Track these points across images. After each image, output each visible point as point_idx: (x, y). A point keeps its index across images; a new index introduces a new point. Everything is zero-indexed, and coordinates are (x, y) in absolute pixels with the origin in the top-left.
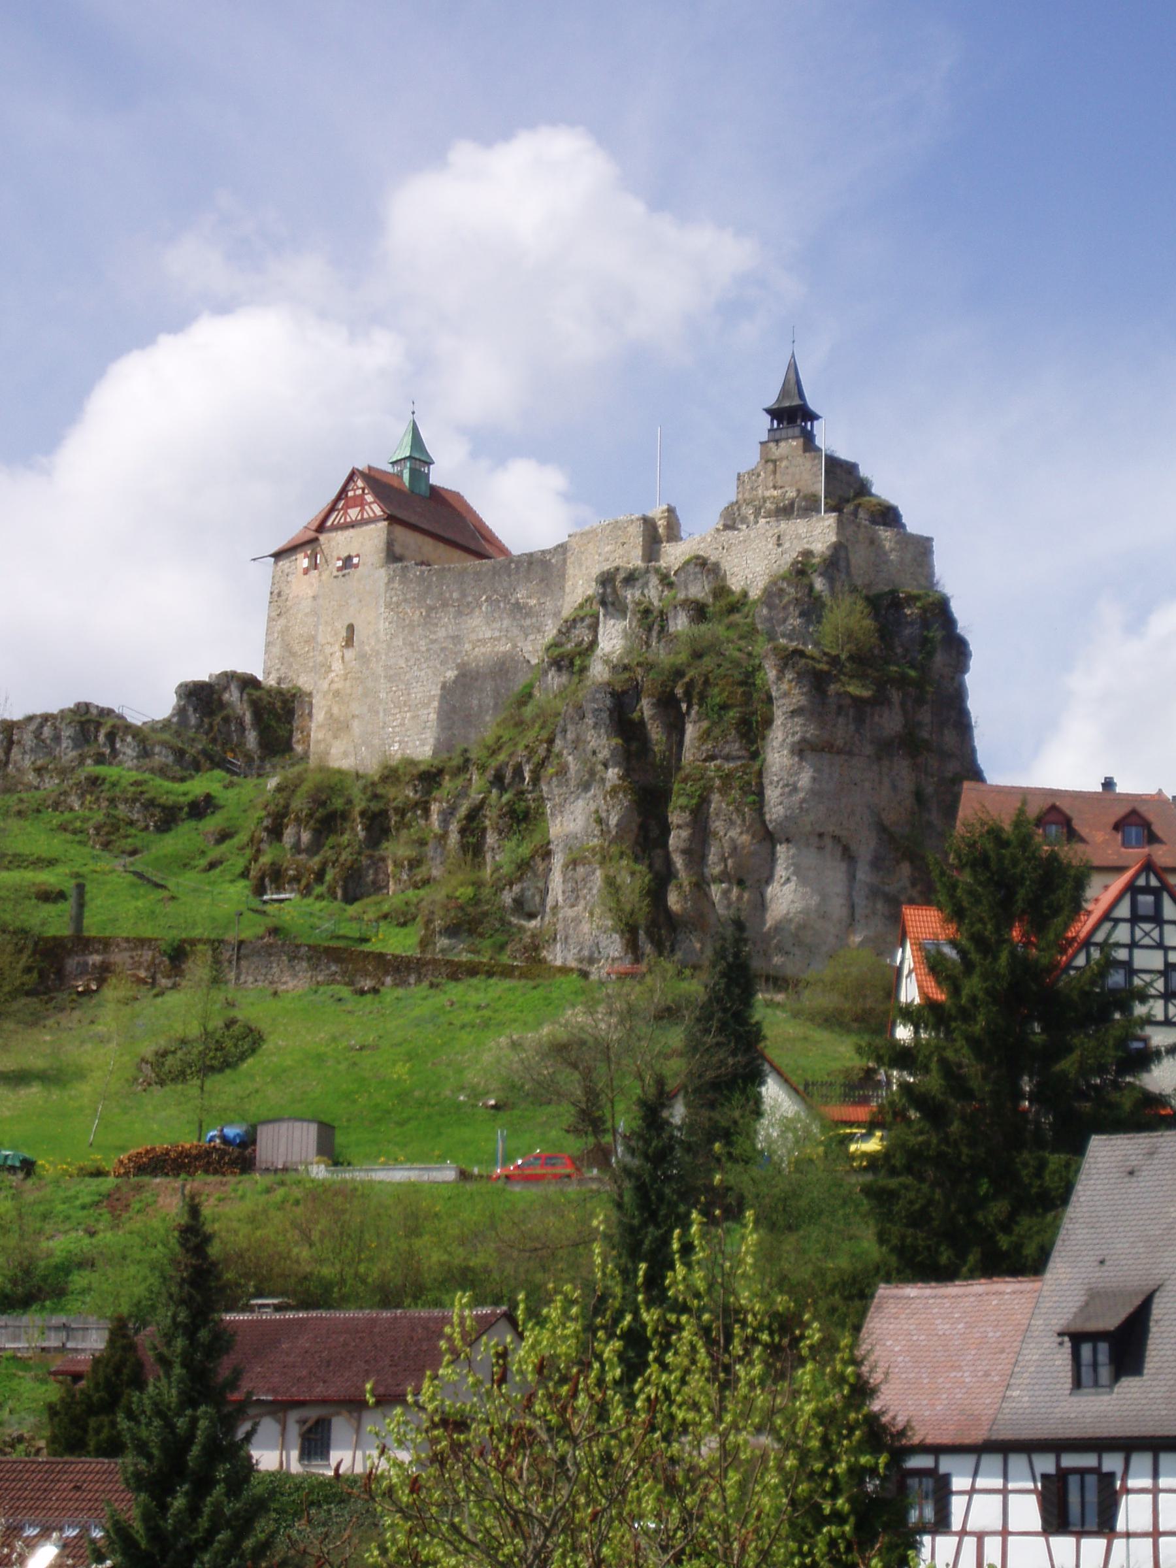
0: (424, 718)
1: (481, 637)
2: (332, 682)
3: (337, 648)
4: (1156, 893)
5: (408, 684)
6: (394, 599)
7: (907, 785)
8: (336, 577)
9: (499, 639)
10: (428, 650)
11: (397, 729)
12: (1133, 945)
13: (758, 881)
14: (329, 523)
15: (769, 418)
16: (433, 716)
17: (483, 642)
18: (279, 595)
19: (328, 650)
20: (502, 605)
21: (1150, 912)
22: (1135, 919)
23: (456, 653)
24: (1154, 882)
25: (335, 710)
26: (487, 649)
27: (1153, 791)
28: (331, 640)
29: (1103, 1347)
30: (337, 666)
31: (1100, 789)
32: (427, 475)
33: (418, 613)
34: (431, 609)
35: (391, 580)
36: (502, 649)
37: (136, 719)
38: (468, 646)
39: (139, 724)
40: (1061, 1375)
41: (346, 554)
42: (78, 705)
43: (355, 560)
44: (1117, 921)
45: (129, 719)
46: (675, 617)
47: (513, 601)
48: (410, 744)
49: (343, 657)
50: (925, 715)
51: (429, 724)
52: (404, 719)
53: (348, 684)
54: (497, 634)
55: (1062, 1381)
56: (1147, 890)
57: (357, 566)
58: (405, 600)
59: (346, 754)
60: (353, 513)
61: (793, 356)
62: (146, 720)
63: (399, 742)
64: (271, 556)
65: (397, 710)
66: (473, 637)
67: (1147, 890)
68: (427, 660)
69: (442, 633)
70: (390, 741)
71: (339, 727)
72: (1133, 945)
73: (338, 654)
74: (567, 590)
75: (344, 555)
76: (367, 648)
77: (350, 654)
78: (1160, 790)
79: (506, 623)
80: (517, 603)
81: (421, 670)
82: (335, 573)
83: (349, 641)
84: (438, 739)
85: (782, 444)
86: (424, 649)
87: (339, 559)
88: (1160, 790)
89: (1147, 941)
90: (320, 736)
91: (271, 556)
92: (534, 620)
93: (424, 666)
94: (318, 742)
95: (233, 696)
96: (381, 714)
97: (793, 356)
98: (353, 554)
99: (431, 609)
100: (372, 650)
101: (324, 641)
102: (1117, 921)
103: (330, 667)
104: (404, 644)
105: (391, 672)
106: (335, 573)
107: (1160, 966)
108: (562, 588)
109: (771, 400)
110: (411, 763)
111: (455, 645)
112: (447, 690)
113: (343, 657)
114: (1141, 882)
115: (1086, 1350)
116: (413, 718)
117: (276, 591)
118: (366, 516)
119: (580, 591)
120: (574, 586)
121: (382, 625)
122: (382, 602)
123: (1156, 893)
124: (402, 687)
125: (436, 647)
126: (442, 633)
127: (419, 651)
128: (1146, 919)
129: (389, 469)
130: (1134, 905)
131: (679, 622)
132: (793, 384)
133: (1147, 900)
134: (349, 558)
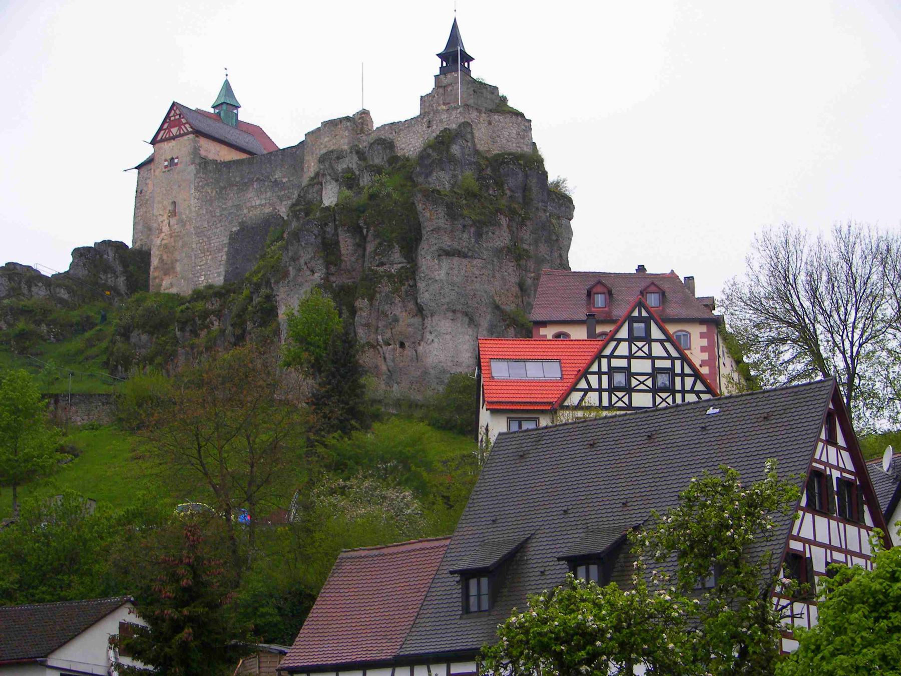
0: (219, 258)
1: (254, 204)
2: (163, 239)
3: (165, 217)
4: (646, 321)
5: (209, 238)
6: (201, 184)
7: (513, 279)
8: (164, 172)
9: (264, 205)
10: (221, 215)
11: (203, 267)
12: (630, 357)
13: (414, 343)
14: (159, 138)
15: (440, 60)
16: (225, 257)
17: (255, 207)
18: (141, 192)
19: (160, 219)
20: (266, 183)
21: (642, 334)
22: (631, 339)
23: (238, 216)
24: (644, 314)
25: (165, 257)
26: (257, 212)
27: (668, 271)
28: (161, 213)
29: (484, 581)
30: (166, 229)
31: (635, 272)
32: (237, 115)
33: (214, 192)
34: (222, 189)
35: (198, 172)
36: (267, 211)
37: (48, 272)
38: (245, 211)
39: (50, 276)
40: (456, 604)
41: (170, 157)
42: (8, 264)
43: (176, 161)
44: (619, 341)
45: (43, 273)
46: (363, 177)
47: (273, 180)
48: (211, 276)
49: (169, 223)
50: (526, 234)
51: (222, 262)
52: (207, 260)
53: (172, 240)
54: (263, 202)
55: (456, 609)
56: (639, 319)
57: (177, 164)
58: (207, 184)
59: (172, 285)
60: (174, 131)
61: (455, 27)
62: (54, 273)
63: (205, 275)
64: (136, 168)
65: (203, 255)
66: (248, 204)
67: (639, 319)
68: (220, 222)
69: (230, 203)
70: (198, 274)
71: (168, 269)
72: (630, 357)
73: (167, 221)
74: (305, 170)
75: (169, 157)
76: (184, 216)
77: (173, 221)
78: (672, 271)
79: (269, 194)
80: (276, 181)
81: (217, 228)
82: (164, 170)
83: (173, 213)
84: (226, 272)
85: (449, 76)
86: (218, 214)
87: (166, 160)
88: (672, 271)
89: (640, 354)
90: (156, 274)
91: (136, 168)
92: (286, 192)
93: (219, 225)
94: (155, 278)
95: (110, 255)
96: (193, 258)
97: (455, 27)
98: (174, 157)
99: (222, 189)
100: (187, 217)
101: (157, 214)
102: (619, 341)
103: (161, 230)
104: (207, 212)
105: (199, 231)
106: (164, 170)
107: (649, 370)
108: (302, 170)
109: (441, 48)
110: (210, 287)
111: (238, 211)
112: (233, 238)
113: (169, 223)
114: (636, 314)
115: (473, 583)
116: (212, 259)
117: (139, 190)
118: (182, 132)
119: (312, 170)
120: (309, 167)
121: (193, 202)
122: (192, 186)
123: (646, 321)
124: (206, 239)
125: (225, 213)
126: (230, 203)
127: (215, 216)
128: (640, 339)
129: (212, 111)
130: (631, 330)
131: (365, 180)
132: (454, 37)
133: (639, 327)
134: (172, 159)
